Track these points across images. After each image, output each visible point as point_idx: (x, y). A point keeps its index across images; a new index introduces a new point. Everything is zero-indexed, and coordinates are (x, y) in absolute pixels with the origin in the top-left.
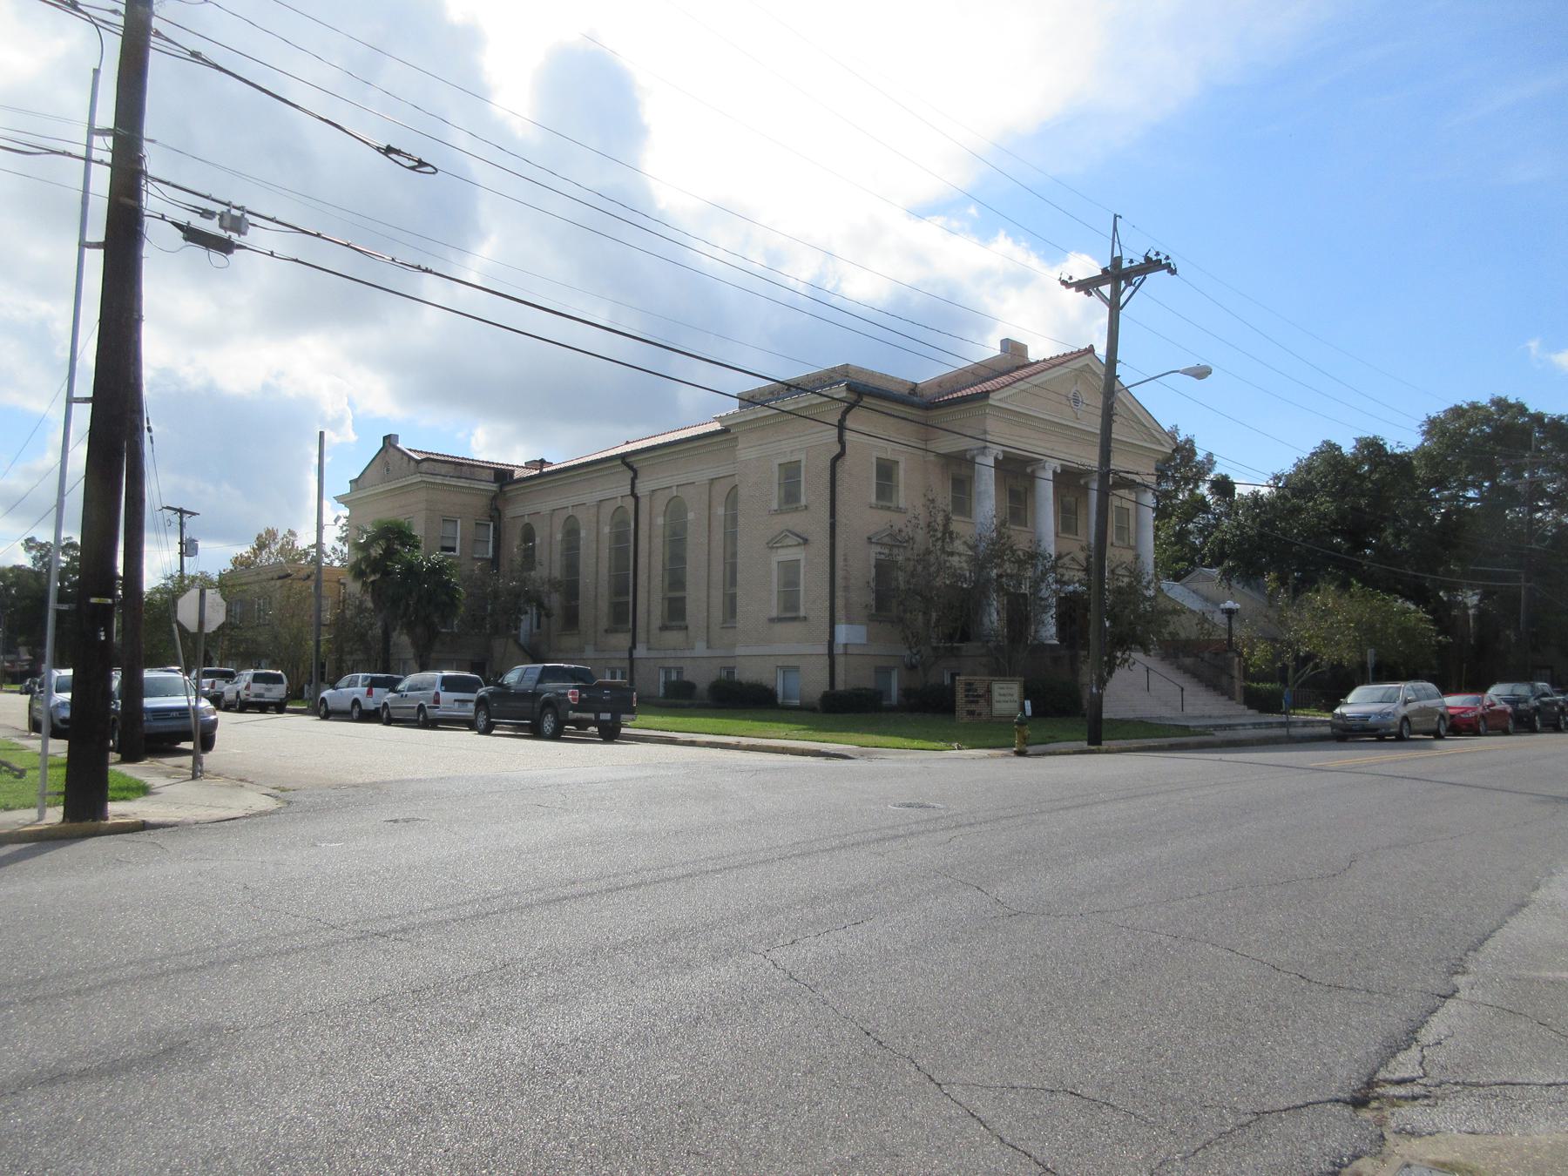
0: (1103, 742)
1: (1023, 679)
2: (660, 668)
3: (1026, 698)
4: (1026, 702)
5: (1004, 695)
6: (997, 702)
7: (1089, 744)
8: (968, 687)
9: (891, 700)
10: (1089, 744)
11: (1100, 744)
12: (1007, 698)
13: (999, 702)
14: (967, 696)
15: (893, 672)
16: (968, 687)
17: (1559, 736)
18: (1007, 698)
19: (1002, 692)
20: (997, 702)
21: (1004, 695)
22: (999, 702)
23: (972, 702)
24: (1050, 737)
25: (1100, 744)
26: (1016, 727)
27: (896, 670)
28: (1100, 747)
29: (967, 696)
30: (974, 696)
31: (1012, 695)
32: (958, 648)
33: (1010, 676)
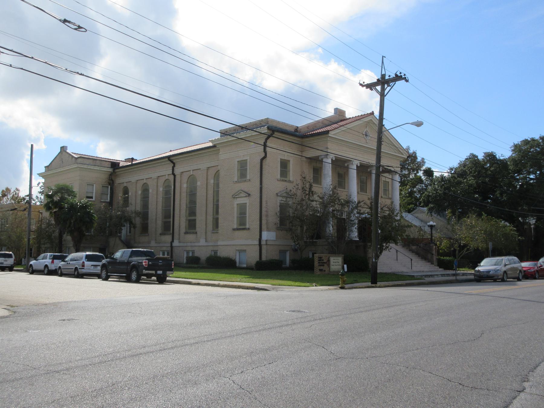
0: (378, 283)
1: (343, 255)
3: (345, 264)
4: (345, 265)
6: (332, 265)
10: (371, 284)
11: (376, 284)
12: (336, 264)
13: (333, 265)
14: (319, 263)
18: (336, 264)
19: (334, 261)
21: (335, 262)
22: (333, 265)
24: (355, 281)
25: (376, 284)
26: (340, 276)
29: (319, 263)
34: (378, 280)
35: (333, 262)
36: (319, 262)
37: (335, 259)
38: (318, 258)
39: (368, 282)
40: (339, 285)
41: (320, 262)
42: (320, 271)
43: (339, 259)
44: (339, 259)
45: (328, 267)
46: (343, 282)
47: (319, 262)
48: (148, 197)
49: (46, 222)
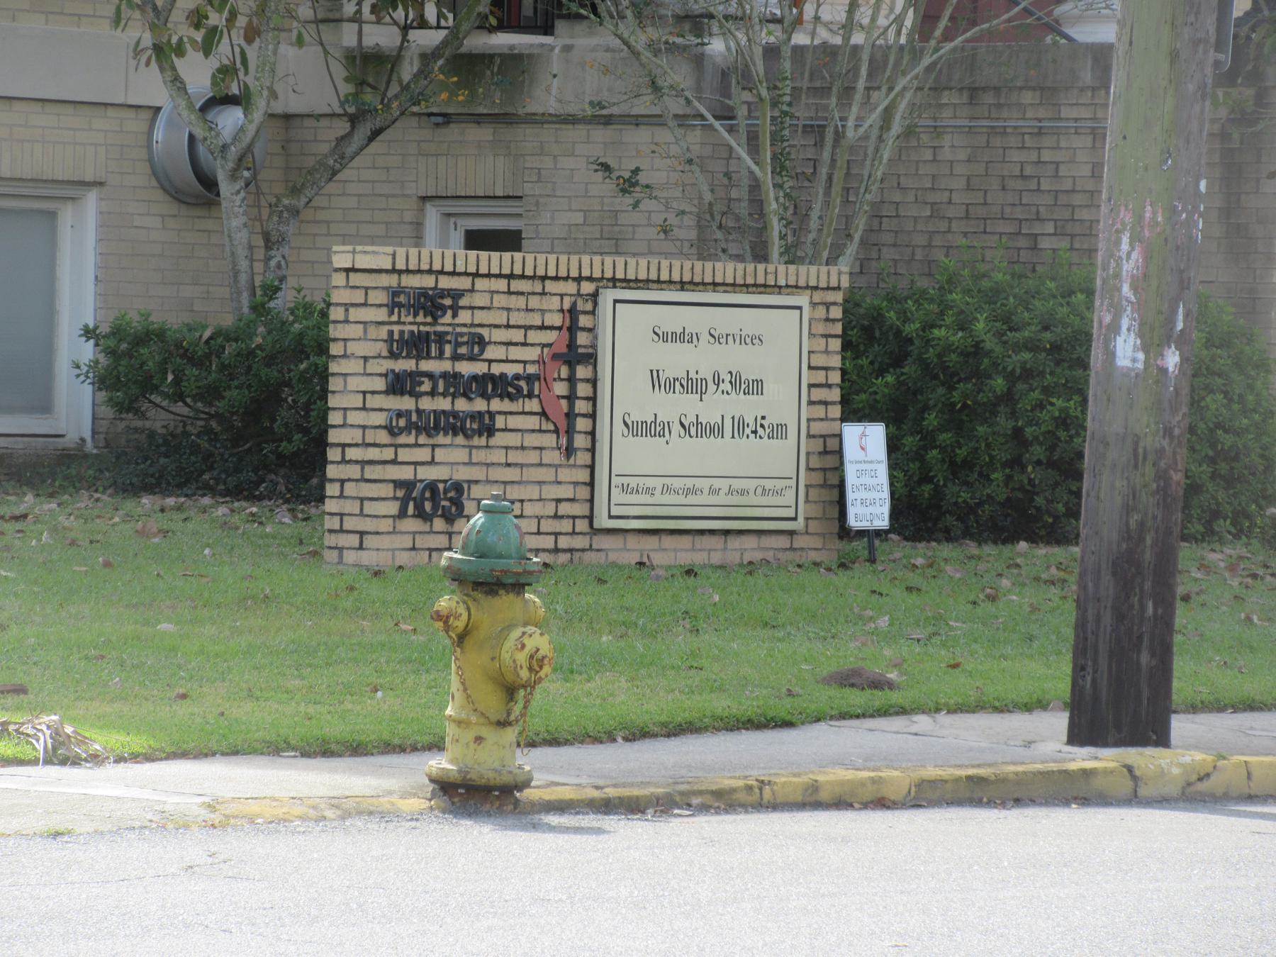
0: (1180, 726)
1: (840, 274)
2: (424, 199)
3: (852, 413)
4: (852, 432)
5: (693, 385)
6: (636, 429)
7: (1080, 734)
8: (411, 324)
9: (45, 406)
10: (1080, 734)
11: (1162, 740)
12: (714, 408)
13: (653, 429)
14: (399, 384)
15: (67, 215)
16: (411, 324)
17: (601, 746)
18: (714, 408)
19: (677, 360)
20: (636, 429)
21: (693, 385)
22: (653, 429)
23: (453, 424)
24: (849, 679)
25: (1162, 740)
26: (445, 602)
27: (91, 200)
28: (1144, 758)
29: (399, 384)
30: (456, 385)
31: (756, 387)
32: (515, 62)
33: (791, 256)
34: (1181, 687)
35: (655, 379)
36: (407, 365)
37: (682, 337)
38: (393, 306)
39: (1031, 706)
40: (436, 746)
41: (415, 376)
42: (421, 514)
43: (757, 340)
44: (757, 340)
45: (570, 451)
46: (492, 702)
47: (407, 365)
48: (1085, 365)
49: (185, 378)
